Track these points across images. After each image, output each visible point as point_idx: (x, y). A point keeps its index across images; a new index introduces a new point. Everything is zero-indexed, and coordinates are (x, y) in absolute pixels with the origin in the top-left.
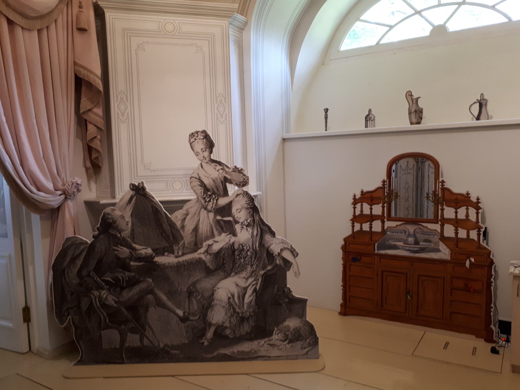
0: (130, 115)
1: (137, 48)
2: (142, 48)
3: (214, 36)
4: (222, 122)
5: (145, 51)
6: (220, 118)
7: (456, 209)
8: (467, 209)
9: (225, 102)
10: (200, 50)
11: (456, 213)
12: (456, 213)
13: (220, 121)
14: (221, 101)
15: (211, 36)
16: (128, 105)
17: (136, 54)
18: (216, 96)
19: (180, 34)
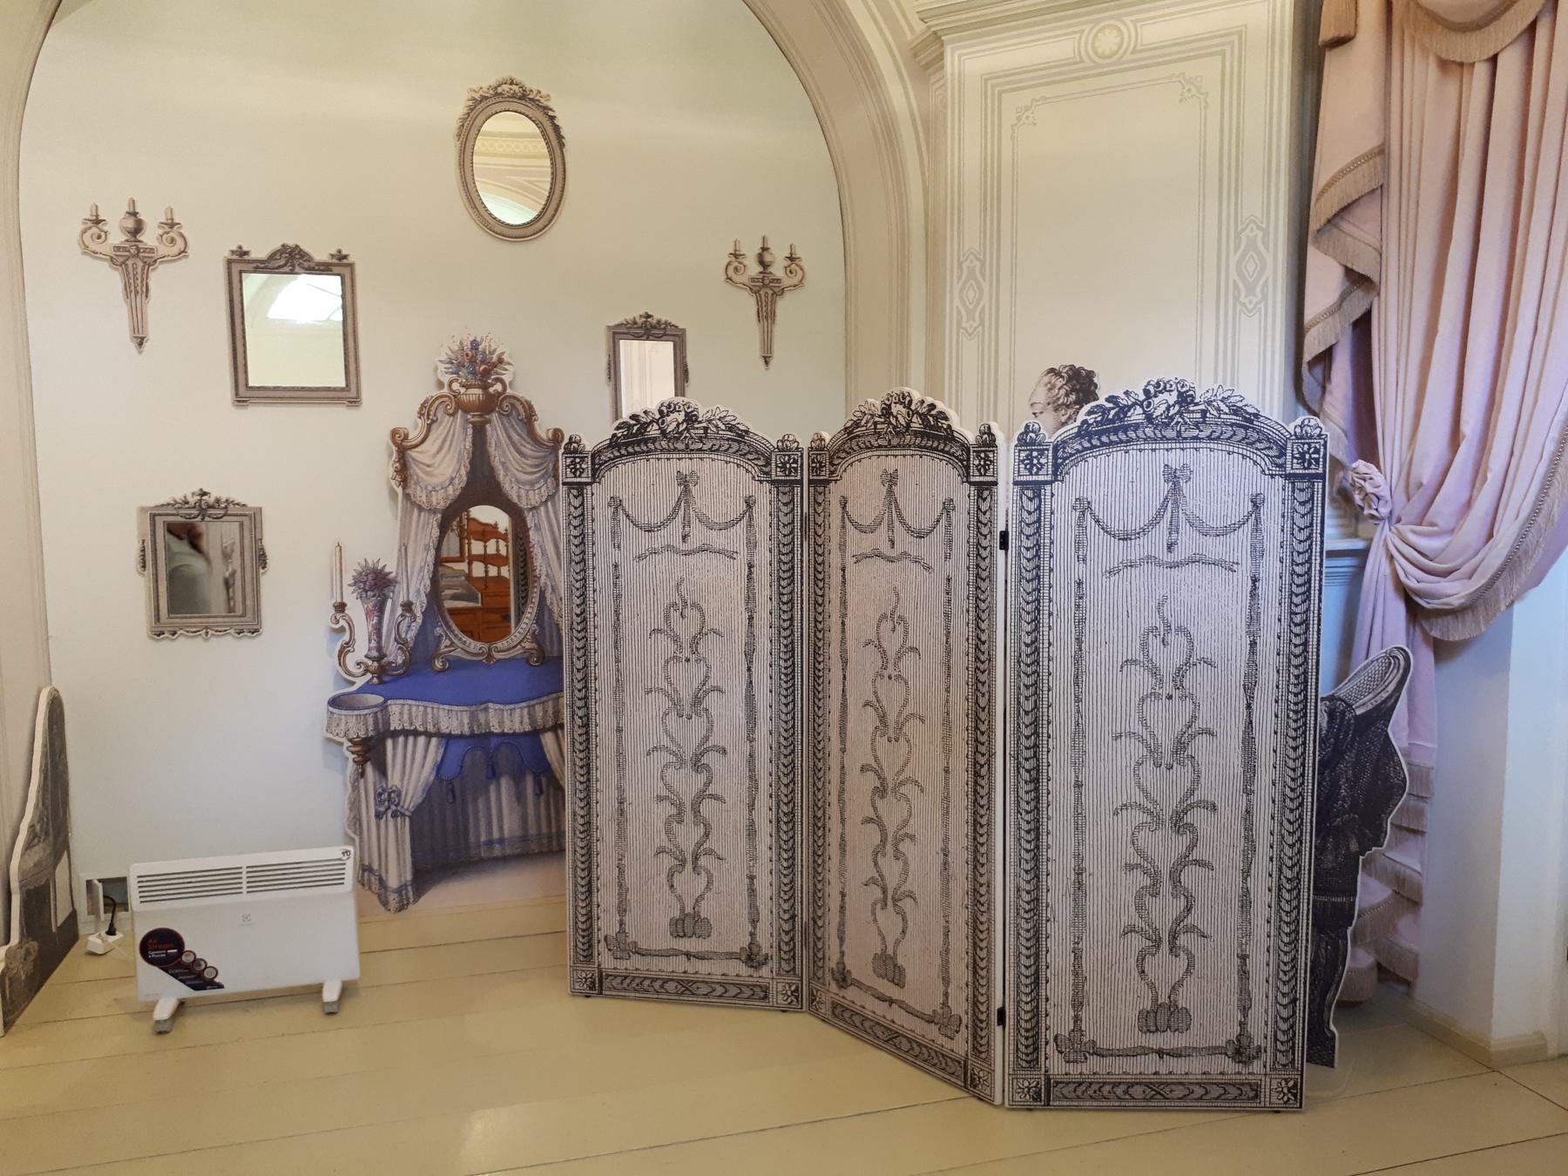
0: (987, 316)
1: (1016, 121)
2: (1027, 118)
3: (986, 80)
4: (970, 331)
5: (1181, 101)
6: (1246, 297)
7: (485, 542)
8: (497, 542)
9: (1264, 244)
10: (1027, 114)
11: (485, 547)
12: (485, 547)
13: (966, 329)
14: (971, 271)
15: (989, 85)
16: (985, 286)
17: (1012, 138)
18: (1236, 226)
19: (1134, 56)
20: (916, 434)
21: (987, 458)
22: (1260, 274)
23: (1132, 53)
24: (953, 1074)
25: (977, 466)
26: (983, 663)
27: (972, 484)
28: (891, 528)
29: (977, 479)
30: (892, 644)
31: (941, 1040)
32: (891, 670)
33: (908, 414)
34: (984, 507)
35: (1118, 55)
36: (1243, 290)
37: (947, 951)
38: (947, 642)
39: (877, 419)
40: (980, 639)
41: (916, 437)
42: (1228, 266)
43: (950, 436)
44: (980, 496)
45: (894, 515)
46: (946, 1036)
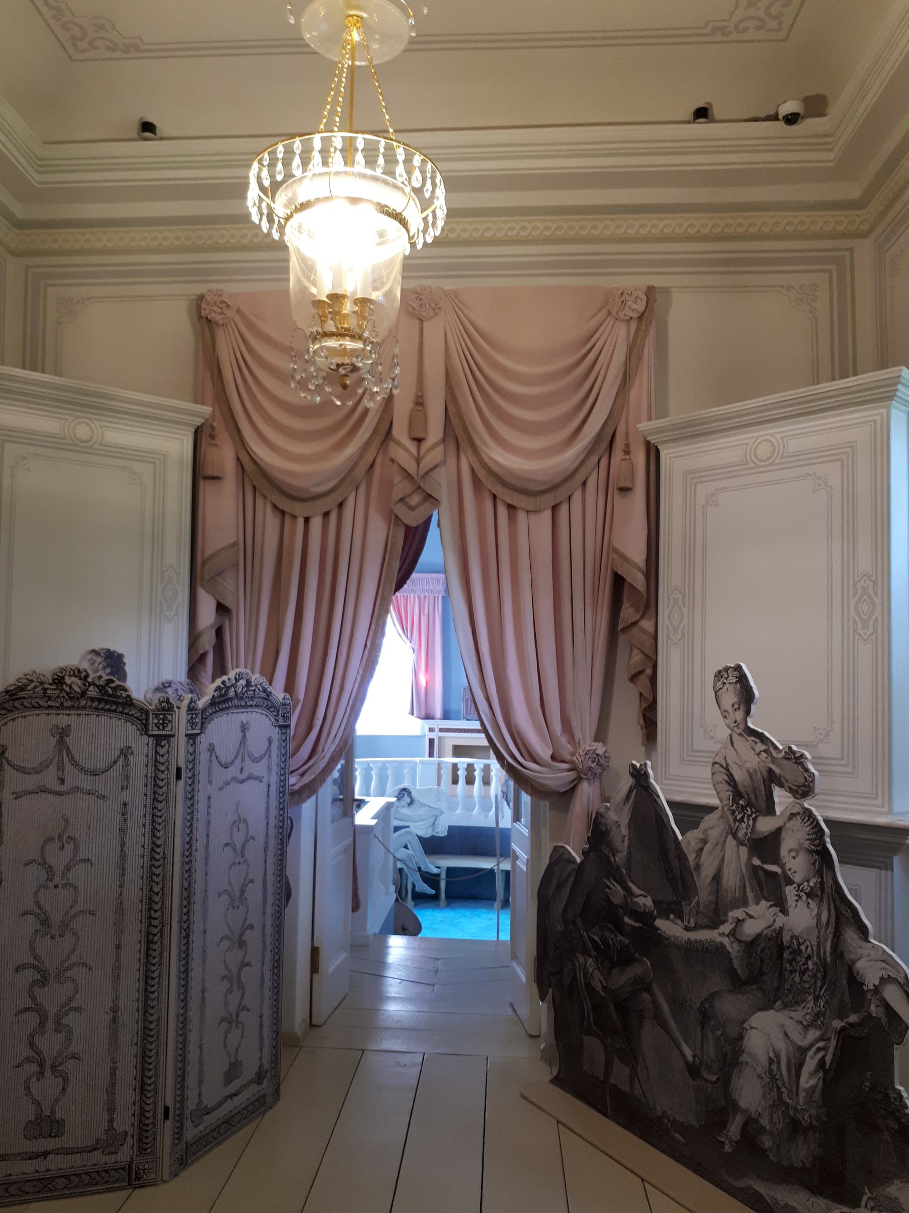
19: (782, 460)
20: (92, 699)
21: (165, 719)
22: (872, 613)
23: (781, 458)
24: (117, 1181)
25: (156, 724)
26: (158, 860)
27: (149, 736)
28: (61, 768)
29: (156, 733)
30: (58, 858)
31: (110, 1159)
32: (57, 880)
33: (84, 685)
34: (162, 751)
35: (773, 459)
36: (860, 625)
37: (113, 1085)
38: (122, 850)
39: (47, 686)
40: (155, 844)
41: (93, 702)
42: (849, 608)
43: (129, 702)
44: (158, 744)
45: (66, 759)
46: (112, 1153)
